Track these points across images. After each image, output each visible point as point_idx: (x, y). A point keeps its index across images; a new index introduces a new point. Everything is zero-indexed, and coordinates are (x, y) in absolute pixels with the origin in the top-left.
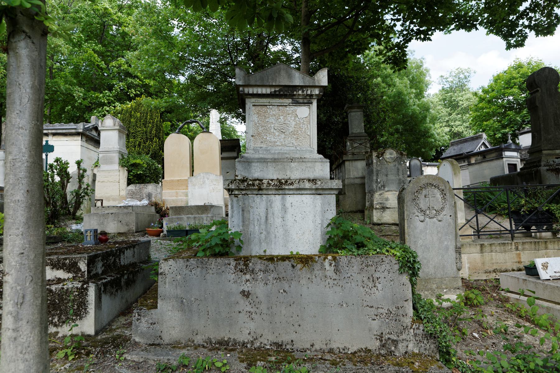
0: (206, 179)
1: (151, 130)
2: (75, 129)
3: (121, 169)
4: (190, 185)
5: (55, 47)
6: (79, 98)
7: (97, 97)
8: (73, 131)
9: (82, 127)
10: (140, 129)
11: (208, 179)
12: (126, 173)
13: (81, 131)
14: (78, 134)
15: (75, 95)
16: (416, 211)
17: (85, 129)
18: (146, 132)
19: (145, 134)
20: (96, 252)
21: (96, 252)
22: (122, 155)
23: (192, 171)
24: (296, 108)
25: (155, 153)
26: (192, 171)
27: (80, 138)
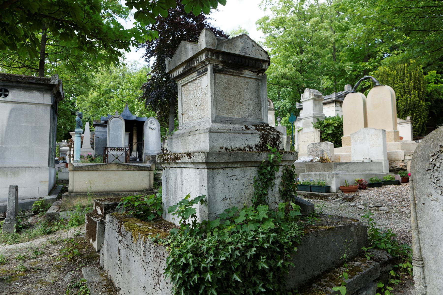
0: (366, 135)
1: (409, 83)
2: (330, 98)
3: (315, 130)
4: (352, 141)
5: (325, 39)
6: (349, 71)
7: (363, 66)
8: (329, 100)
9: (334, 96)
10: (397, 85)
11: (368, 134)
12: (319, 134)
13: (334, 99)
14: (333, 102)
15: (346, 69)
16: (433, 191)
17: (337, 97)
18: (404, 87)
19: (402, 89)
20: (114, 196)
21: (114, 196)
22: (318, 119)
23: (81, 145)
24: (240, 54)
25: (415, 105)
26: (81, 145)
27: (334, 104)
